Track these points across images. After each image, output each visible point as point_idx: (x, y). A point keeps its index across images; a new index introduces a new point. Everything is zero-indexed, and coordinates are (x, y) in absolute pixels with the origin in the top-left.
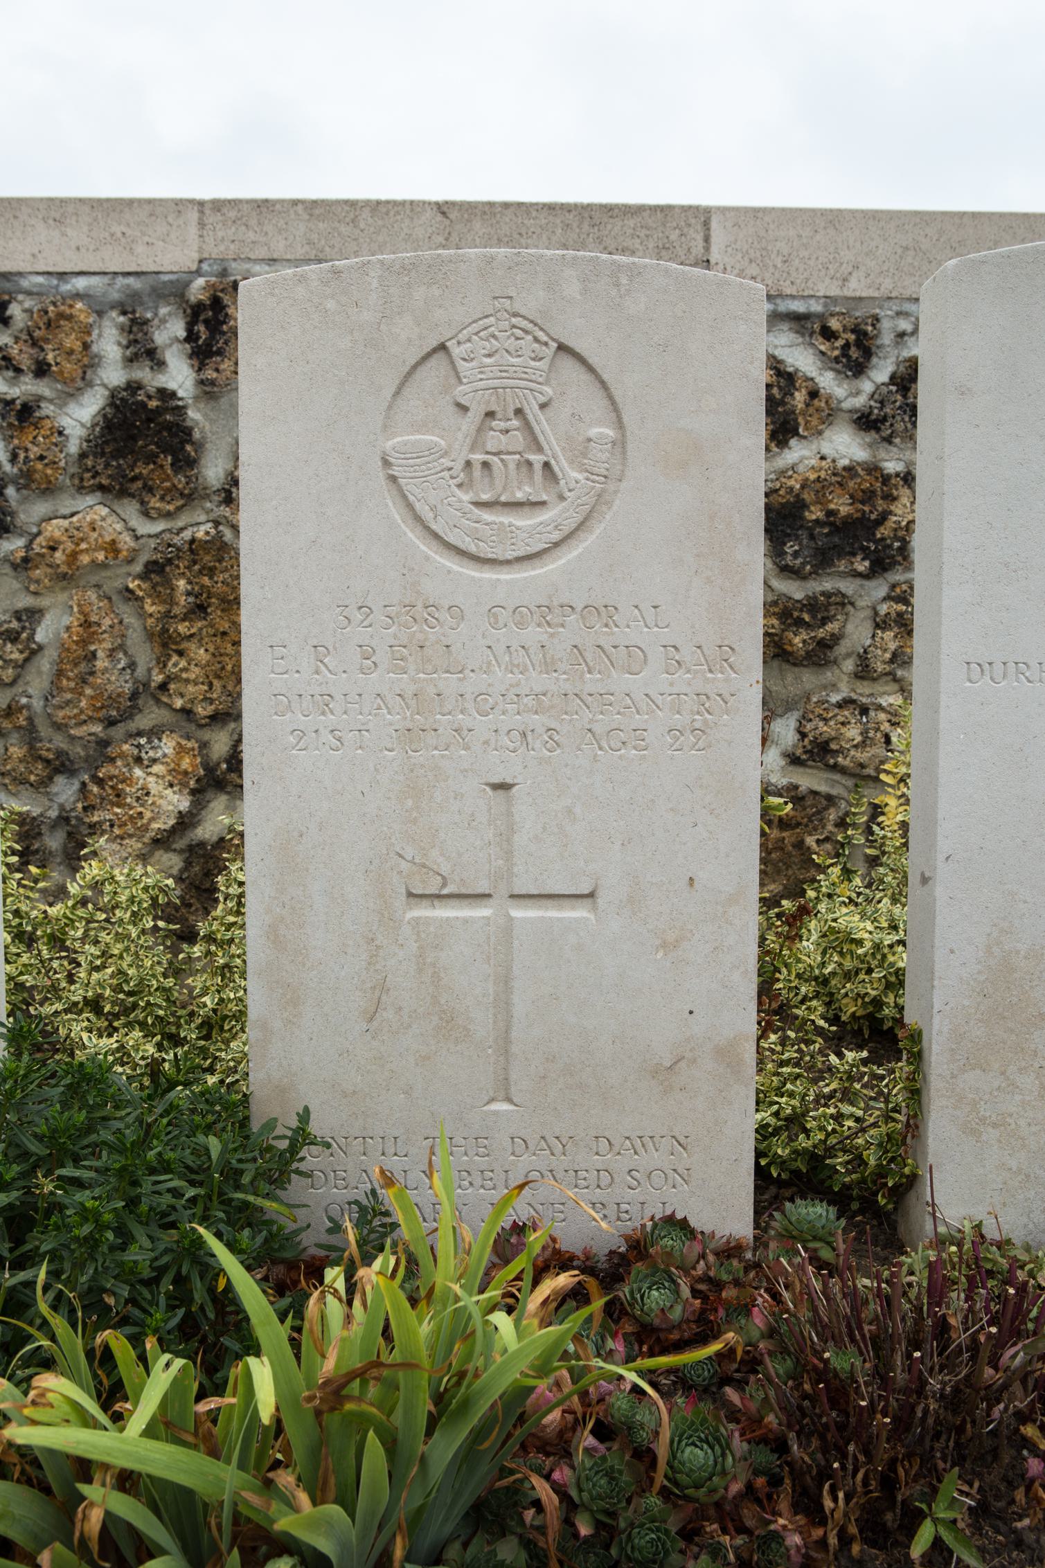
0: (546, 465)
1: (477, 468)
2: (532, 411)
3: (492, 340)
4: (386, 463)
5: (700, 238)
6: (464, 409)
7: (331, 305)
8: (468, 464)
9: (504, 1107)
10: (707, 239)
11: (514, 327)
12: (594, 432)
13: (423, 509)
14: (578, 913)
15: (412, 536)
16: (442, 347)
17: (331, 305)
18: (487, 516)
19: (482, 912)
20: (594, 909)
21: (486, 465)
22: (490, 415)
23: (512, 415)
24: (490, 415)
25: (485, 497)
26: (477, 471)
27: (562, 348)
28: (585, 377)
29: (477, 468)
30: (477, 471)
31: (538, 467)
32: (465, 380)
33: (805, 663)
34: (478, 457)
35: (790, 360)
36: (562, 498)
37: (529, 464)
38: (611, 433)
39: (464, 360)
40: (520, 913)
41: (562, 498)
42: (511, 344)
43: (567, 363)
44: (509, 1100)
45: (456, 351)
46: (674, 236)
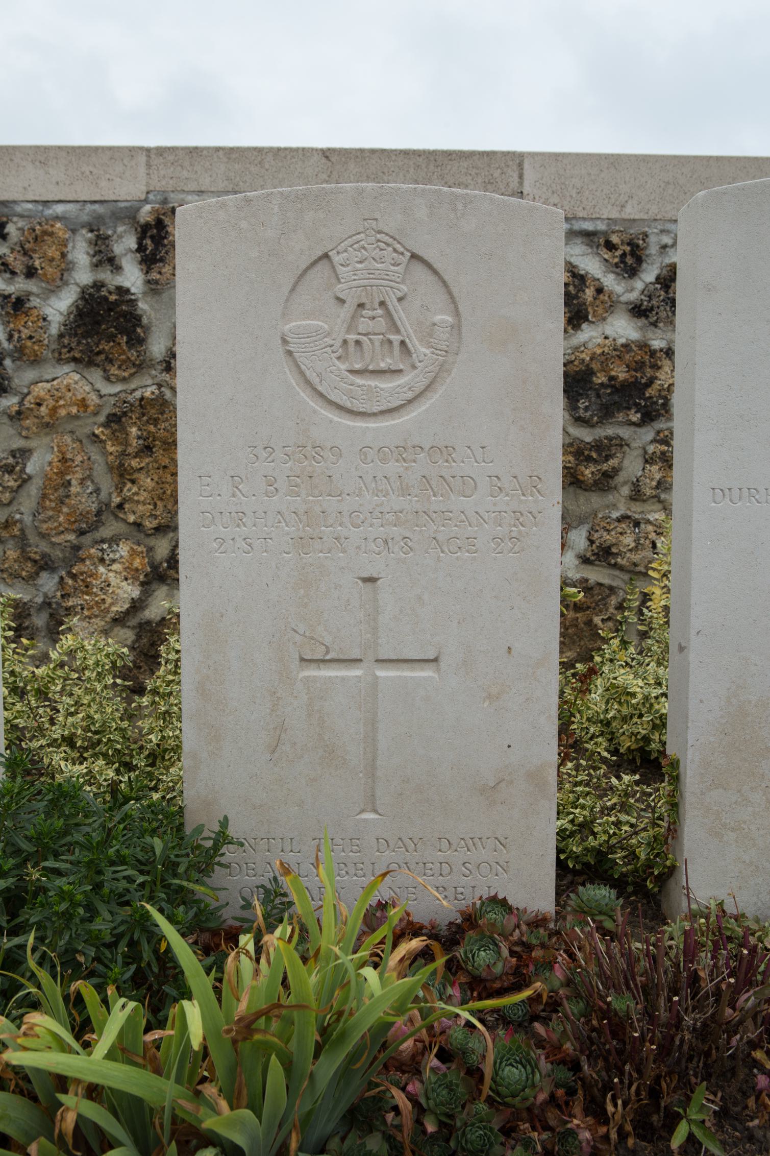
0: (403, 343)
1: (351, 345)
2: (392, 303)
3: (363, 251)
4: (285, 342)
5: (516, 179)
6: (342, 301)
7: (244, 225)
8: (345, 342)
9: (372, 816)
10: (521, 176)
11: (379, 241)
12: (438, 318)
13: (311, 375)
14: (426, 673)
15: (304, 395)
16: (326, 256)
17: (244, 225)
18: (359, 381)
19: (355, 672)
20: (438, 670)
21: (358, 343)
22: (361, 306)
23: (377, 306)
24: (361, 306)
25: (357, 366)
26: (352, 347)
27: (414, 256)
28: (431, 278)
29: (351, 345)
30: (352, 347)
31: (396, 344)
32: (342, 280)
33: (593, 489)
34: (352, 337)
35: (582, 266)
36: (414, 367)
37: (390, 342)
38: (450, 319)
39: (342, 265)
40: (382, 673)
41: (414, 367)
42: (376, 253)
43: (418, 270)
44: (375, 811)
45: (336, 259)
46: (497, 174)
